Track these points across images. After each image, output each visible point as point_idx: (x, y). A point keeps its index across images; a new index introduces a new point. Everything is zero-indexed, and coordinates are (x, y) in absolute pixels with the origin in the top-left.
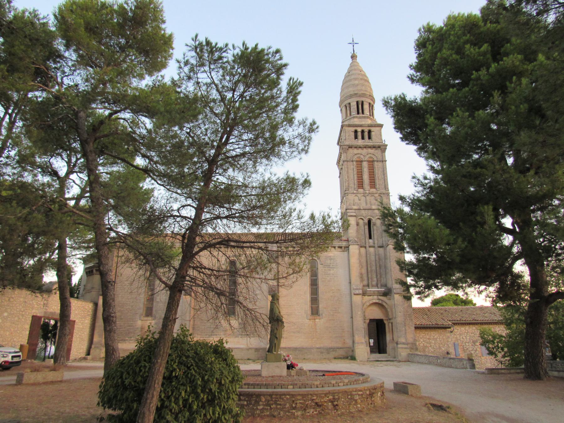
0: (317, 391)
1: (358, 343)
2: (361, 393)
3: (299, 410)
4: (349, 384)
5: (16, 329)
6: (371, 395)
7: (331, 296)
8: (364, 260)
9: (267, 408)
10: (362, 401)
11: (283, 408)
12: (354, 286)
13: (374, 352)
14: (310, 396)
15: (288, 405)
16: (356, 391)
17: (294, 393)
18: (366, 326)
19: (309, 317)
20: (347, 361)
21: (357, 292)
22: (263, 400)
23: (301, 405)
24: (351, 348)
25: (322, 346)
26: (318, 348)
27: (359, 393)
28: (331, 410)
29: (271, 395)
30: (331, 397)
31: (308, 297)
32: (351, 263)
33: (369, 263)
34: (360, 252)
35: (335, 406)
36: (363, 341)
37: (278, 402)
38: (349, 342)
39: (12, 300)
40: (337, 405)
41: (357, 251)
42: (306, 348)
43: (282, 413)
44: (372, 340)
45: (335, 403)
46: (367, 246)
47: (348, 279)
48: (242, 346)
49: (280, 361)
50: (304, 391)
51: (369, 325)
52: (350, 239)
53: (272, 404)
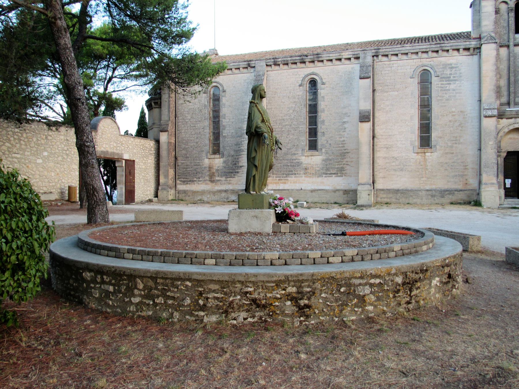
0: (255, 276)
1: (486, 184)
2: (378, 281)
3: (214, 313)
4: (359, 258)
5: (62, 169)
6: (410, 284)
7: (450, 121)
8: (504, 66)
9: (147, 302)
10: (378, 299)
11: (179, 306)
12: (485, 105)
13: (512, 197)
14: (238, 285)
15: (188, 301)
16: (361, 278)
17: (200, 278)
18: (501, 161)
19: (417, 150)
20: (468, 207)
21: (490, 113)
22: (141, 286)
23: (217, 302)
24: (475, 190)
25: (434, 187)
26: (427, 190)
27: (372, 281)
28: (292, 316)
29: (155, 277)
30: (292, 290)
31: (416, 123)
32: (483, 72)
33: (512, 69)
34: (498, 54)
35: (303, 310)
36: (494, 181)
37: (169, 294)
38: (473, 183)
39: (49, 138)
40: (308, 306)
41: (494, 53)
42: (411, 190)
43: (176, 315)
44: (510, 180)
45: (302, 303)
46: (511, 44)
47: (477, 95)
48: (327, 188)
49: (262, 207)
50: (223, 275)
51: (505, 159)
52: (482, 36)
53: (158, 297)
